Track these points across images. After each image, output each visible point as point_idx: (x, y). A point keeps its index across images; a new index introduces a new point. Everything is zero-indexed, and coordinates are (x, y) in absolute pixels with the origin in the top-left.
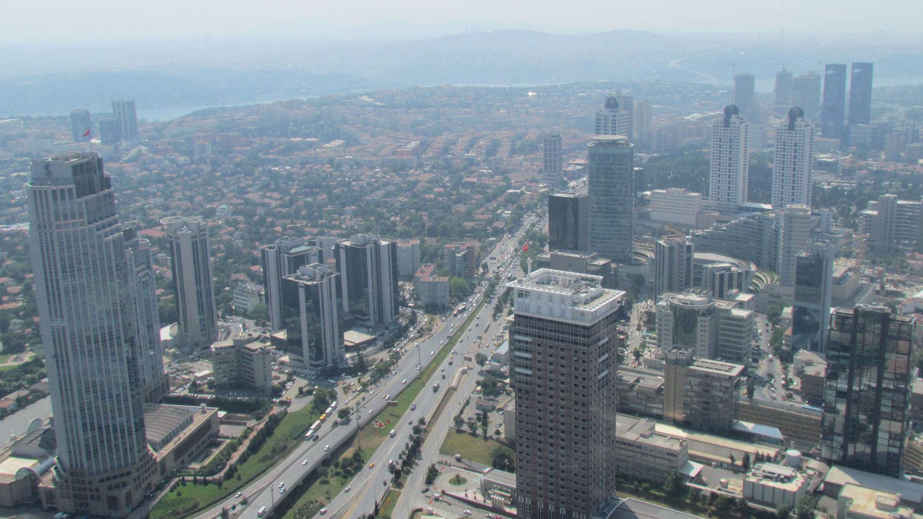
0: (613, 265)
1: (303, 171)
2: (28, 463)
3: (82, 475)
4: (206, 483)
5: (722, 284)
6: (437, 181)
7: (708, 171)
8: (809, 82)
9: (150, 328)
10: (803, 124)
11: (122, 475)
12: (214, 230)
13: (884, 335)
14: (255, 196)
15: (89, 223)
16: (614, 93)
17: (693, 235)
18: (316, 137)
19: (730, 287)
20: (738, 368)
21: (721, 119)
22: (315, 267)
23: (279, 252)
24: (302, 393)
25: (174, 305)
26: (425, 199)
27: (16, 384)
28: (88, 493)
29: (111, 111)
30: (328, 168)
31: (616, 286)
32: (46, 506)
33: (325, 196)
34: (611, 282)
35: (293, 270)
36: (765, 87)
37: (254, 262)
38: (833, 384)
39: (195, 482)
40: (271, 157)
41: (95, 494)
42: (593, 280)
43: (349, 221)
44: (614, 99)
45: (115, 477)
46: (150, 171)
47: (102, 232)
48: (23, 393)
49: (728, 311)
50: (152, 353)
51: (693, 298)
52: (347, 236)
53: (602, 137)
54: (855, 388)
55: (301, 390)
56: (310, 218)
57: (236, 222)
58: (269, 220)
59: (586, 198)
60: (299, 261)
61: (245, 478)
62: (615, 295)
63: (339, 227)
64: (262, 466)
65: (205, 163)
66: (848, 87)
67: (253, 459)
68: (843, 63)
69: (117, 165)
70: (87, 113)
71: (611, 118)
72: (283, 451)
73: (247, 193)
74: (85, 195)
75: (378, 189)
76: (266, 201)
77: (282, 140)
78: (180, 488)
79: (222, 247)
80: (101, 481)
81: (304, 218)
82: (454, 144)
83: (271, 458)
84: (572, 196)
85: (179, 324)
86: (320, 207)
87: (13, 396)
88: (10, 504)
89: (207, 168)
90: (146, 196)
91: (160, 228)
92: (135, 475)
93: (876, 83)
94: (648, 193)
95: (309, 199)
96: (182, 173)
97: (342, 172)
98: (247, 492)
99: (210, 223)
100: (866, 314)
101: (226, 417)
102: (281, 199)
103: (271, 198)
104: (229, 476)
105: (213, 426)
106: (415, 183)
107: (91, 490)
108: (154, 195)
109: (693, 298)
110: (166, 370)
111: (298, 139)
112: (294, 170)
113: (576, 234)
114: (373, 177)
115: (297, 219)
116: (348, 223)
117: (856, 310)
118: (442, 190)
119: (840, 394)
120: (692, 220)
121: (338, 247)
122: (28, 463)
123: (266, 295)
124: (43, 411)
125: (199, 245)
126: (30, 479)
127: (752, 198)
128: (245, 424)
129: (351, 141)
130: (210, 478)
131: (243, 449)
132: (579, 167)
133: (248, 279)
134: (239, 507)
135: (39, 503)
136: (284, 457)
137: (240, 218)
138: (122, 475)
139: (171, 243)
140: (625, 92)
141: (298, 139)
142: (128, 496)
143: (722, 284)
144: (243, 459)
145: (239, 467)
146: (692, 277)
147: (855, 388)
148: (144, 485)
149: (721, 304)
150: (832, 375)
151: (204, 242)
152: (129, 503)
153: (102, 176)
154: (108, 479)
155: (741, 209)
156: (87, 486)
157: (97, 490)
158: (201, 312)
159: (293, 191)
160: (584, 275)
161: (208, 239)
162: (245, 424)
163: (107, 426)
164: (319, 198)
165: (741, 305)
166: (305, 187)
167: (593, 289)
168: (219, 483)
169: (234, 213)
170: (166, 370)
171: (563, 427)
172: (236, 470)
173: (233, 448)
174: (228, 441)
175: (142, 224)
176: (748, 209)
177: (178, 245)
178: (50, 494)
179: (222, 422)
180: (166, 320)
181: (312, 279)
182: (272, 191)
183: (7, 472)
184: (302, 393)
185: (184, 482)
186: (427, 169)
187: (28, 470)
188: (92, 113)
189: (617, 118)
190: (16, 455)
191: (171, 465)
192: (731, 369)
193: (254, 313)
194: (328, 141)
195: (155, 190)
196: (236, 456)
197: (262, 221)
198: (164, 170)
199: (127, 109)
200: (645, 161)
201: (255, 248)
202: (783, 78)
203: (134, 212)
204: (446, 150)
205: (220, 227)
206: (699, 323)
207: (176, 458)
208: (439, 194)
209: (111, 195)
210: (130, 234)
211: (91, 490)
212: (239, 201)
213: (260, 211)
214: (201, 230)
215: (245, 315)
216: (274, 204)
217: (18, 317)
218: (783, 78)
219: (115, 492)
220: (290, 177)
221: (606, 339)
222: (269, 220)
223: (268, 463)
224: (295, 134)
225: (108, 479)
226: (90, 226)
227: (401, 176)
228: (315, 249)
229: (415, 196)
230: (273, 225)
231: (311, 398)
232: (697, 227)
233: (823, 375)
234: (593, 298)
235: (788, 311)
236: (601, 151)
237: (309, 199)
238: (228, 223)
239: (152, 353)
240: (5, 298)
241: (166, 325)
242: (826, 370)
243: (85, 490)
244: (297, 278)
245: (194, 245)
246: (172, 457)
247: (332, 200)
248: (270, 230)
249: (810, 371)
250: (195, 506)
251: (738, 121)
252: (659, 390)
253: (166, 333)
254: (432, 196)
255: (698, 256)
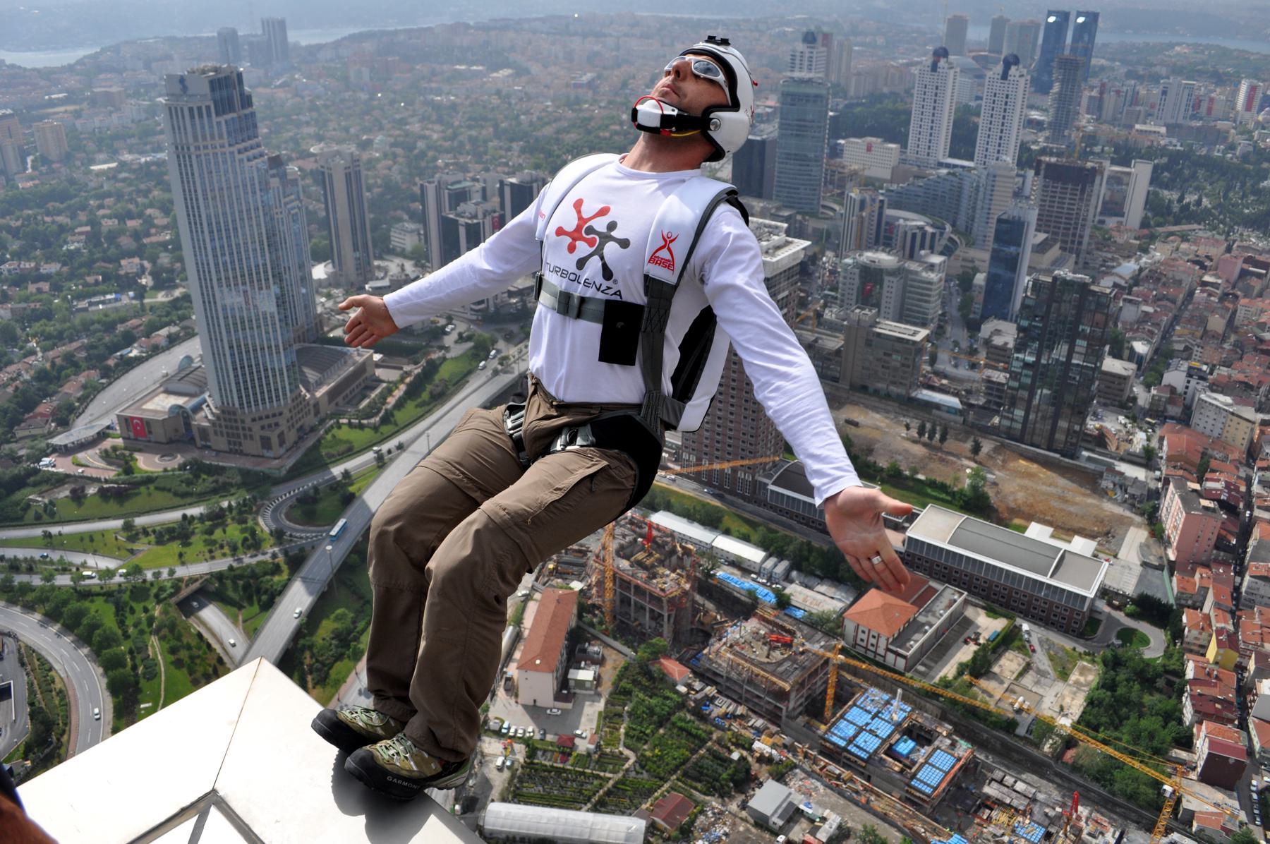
0: (799, 217)
1: (467, 103)
2: (181, 401)
3: (234, 413)
4: (361, 427)
5: (913, 245)
6: (613, 118)
7: (909, 121)
8: (1027, 29)
9: (301, 267)
10: (1018, 74)
11: (274, 415)
12: (371, 164)
13: (1080, 308)
14: (415, 127)
15: (230, 145)
16: (813, 28)
17: (888, 190)
18: (482, 65)
19: (922, 247)
20: (923, 333)
21: (929, 62)
22: (477, 204)
23: (438, 189)
24: (461, 339)
25: (327, 242)
26: (599, 137)
27: (167, 319)
28: (241, 432)
29: (260, 32)
30: (495, 101)
31: (800, 236)
32: (199, 443)
33: (491, 130)
34: (796, 231)
35: (454, 206)
36: (978, 34)
37: (413, 198)
38: (1021, 356)
39: (350, 425)
40: (433, 85)
41: (248, 433)
42: (777, 227)
43: (515, 160)
44: (813, 34)
45: (267, 417)
46: (303, 97)
47: (244, 156)
48: (174, 329)
49: (916, 273)
50: (304, 291)
51: (884, 258)
52: (512, 174)
53: (797, 74)
54: (1043, 361)
55: (460, 335)
56: (478, 157)
57: (395, 156)
58: (431, 154)
59: (774, 142)
60: (461, 197)
61: (401, 424)
62: (800, 245)
63: (506, 164)
64: (420, 411)
65: (362, 90)
66: (1069, 39)
67: (410, 405)
68: (1066, 9)
69: (268, 91)
70: (234, 32)
71: (807, 55)
72: (440, 397)
73: (406, 124)
74: (224, 113)
75: (548, 123)
76: (427, 133)
77: (445, 67)
78: (335, 431)
79: (379, 181)
80: (254, 420)
81: (468, 154)
82: (634, 77)
83: (429, 404)
84: (759, 138)
85: (333, 262)
86: (485, 142)
87: (164, 332)
88: (164, 440)
89: (363, 96)
90: (299, 125)
91: (312, 159)
92: (289, 415)
93: (1100, 39)
94: (842, 142)
95: (473, 133)
96: (337, 100)
97: (510, 104)
98: (403, 437)
99: (365, 156)
100: (1066, 283)
101: (382, 360)
102: (442, 132)
103: (432, 130)
104: (386, 419)
105: (369, 369)
106: (591, 119)
107: (244, 429)
108: (308, 124)
109: (884, 258)
110: (319, 310)
111: (463, 67)
112: (459, 101)
113: (761, 185)
114: (544, 110)
115: (461, 153)
116: (515, 159)
117: (1055, 279)
118: (617, 128)
119: (1027, 365)
120: (886, 174)
121: (502, 183)
122: (181, 401)
123: (426, 235)
124: (194, 348)
125: (353, 177)
126: (181, 416)
127: (951, 155)
128: (401, 368)
129: (520, 72)
130: (365, 422)
131: (398, 393)
132: (769, 110)
133: (406, 217)
134: (395, 452)
135: (192, 440)
136: (443, 404)
137: (399, 151)
138: (274, 415)
139: (323, 173)
140: (825, 29)
141: (463, 67)
142: (281, 435)
143: (913, 245)
144: (400, 404)
145: (396, 413)
146: (884, 236)
147: (1043, 361)
148: (297, 426)
149: (913, 266)
150: (1020, 347)
151: (358, 173)
152: (282, 443)
153: (242, 93)
154: (261, 418)
155: (941, 165)
156: (239, 425)
157: (250, 429)
158: (356, 249)
159: (456, 123)
160: (767, 222)
161: (364, 173)
162: (401, 368)
163: (273, 370)
164: (484, 132)
165: (931, 267)
166: (470, 119)
167: (776, 238)
168: (375, 428)
169: (392, 145)
170: (319, 310)
171: (734, 384)
172: (393, 415)
173: (389, 391)
174: (384, 385)
175: (294, 155)
176: (948, 166)
177: (330, 176)
178: (203, 432)
179: (378, 365)
180: (319, 257)
181: (472, 218)
182: (433, 123)
183: (159, 408)
184: (461, 339)
185: (339, 426)
186: (602, 104)
187: (180, 407)
188: (240, 33)
189: (815, 55)
190: (168, 392)
191: (326, 409)
192: (915, 333)
193: (412, 253)
194: (496, 70)
195: (308, 119)
196: (391, 401)
197: (423, 154)
198: (318, 97)
199: (277, 28)
200: (841, 107)
201: (415, 184)
202: (998, 26)
203: (286, 142)
204: (624, 85)
205: (378, 160)
206: (886, 284)
207: (330, 402)
208: (616, 133)
209: (253, 114)
210: (276, 162)
211: (244, 429)
212: (398, 132)
213: (421, 145)
214: (355, 160)
215: (403, 254)
216: (435, 136)
217: (166, 250)
218: (998, 26)
219: (266, 433)
220: (454, 107)
221: (786, 293)
222: (431, 154)
223: (427, 408)
224: (460, 62)
225: (261, 418)
226: (232, 149)
227: (574, 111)
228: (478, 186)
229: (589, 132)
230: (435, 159)
231: (470, 344)
232: (891, 181)
233: (1011, 345)
234: (778, 248)
235: (980, 279)
236: (793, 89)
237: (473, 133)
238: (385, 156)
239: (304, 291)
240: (153, 231)
241: (320, 262)
242: (1016, 340)
243: (237, 428)
244: (457, 215)
245: (348, 176)
246: (326, 398)
247: (498, 134)
248: (431, 165)
249: (998, 341)
250: (350, 449)
251: (946, 66)
252: (838, 352)
253: (320, 272)
254: (607, 134)
255: (890, 212)
